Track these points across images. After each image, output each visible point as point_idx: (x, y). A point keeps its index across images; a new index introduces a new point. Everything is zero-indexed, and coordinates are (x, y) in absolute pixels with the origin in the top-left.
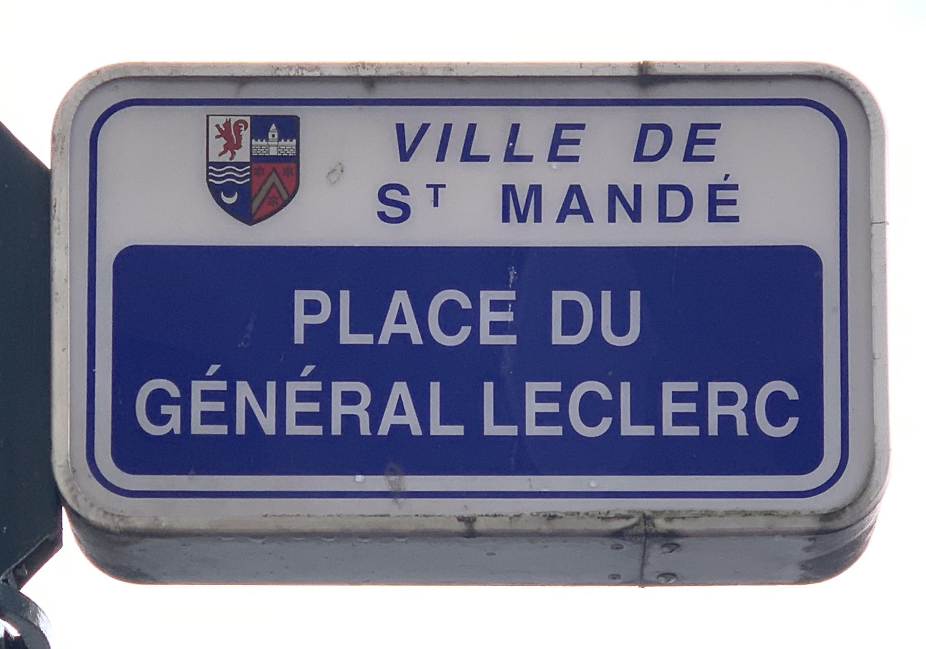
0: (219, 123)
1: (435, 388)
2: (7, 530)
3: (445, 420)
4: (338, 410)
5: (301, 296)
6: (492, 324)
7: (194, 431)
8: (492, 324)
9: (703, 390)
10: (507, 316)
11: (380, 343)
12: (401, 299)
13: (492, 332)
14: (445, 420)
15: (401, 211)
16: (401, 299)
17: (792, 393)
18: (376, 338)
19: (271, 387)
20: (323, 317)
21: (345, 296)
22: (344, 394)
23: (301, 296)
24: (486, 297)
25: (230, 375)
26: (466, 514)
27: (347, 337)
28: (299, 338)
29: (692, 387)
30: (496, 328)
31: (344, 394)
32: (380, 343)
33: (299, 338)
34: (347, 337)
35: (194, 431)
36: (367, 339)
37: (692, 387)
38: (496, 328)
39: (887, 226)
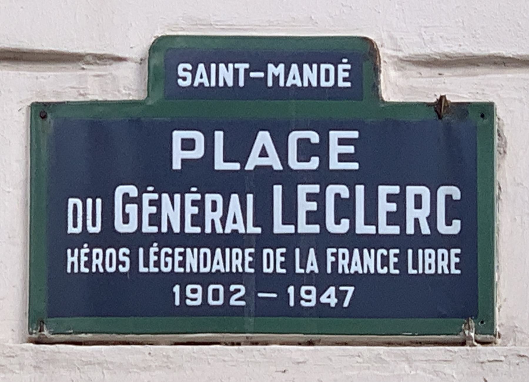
3: (255, 225)
4: (411, 213)
5: (178, 136)
6: (340, 155)
7: (358, 231)
8: (340, 155)
10: (350, 149)
11: (247, 168)
13: (340, 161)
14: (255, 225)
18: (243, 165)
19: (177, 197)
21: (219, 136)
23: (178, 136)
24: (334, 136)
25: (159, 191)
26: (331, 296)
27: (220, 164)
30: (342, 158)
32: (247, 168)
34: (220, 164)
35: (358, 231)
36: (236, 166)
38: (342, 158)
39: (452, 99)
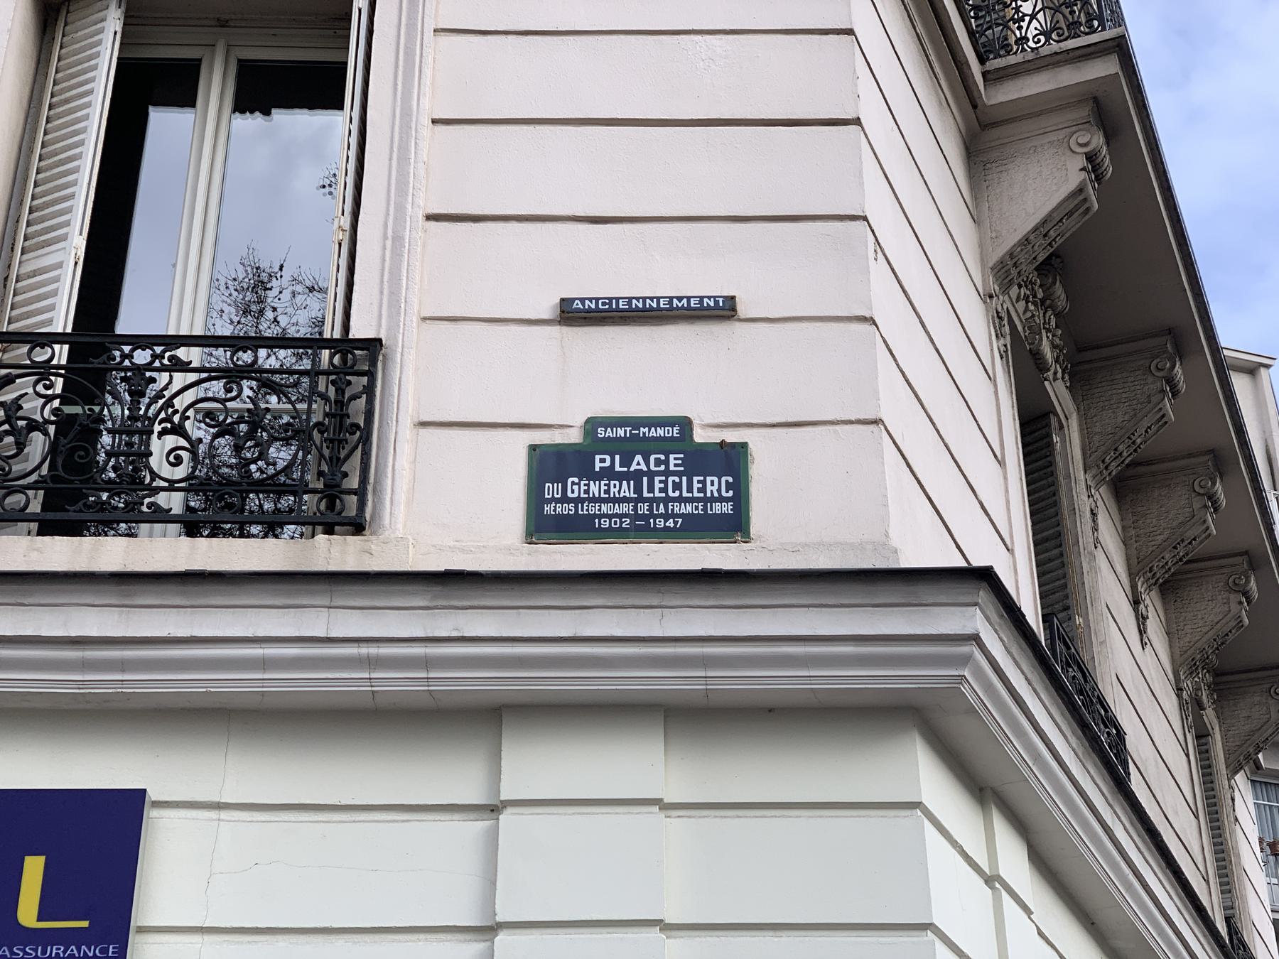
0: (315, 188)
1: (632, 482)
2: (92, 497)
5: (598, 457)
7: (684, 496)
9: (705, 480)
12: (638, 458)
15: (637, 456)
16: (638, 458)
17: (731, 480)
18: (629, 469)
20: (608, 464)
22: (600, 459)
23: (598, 457)
24: (672, 456)
27: (617, 468)
28: (636, 496)
29: (702, 478)
31: (600, 459)
33: (636, 496)
34: (617, 468)
35: (684, 496)
37: (702, 478)
